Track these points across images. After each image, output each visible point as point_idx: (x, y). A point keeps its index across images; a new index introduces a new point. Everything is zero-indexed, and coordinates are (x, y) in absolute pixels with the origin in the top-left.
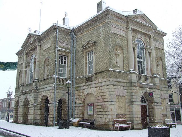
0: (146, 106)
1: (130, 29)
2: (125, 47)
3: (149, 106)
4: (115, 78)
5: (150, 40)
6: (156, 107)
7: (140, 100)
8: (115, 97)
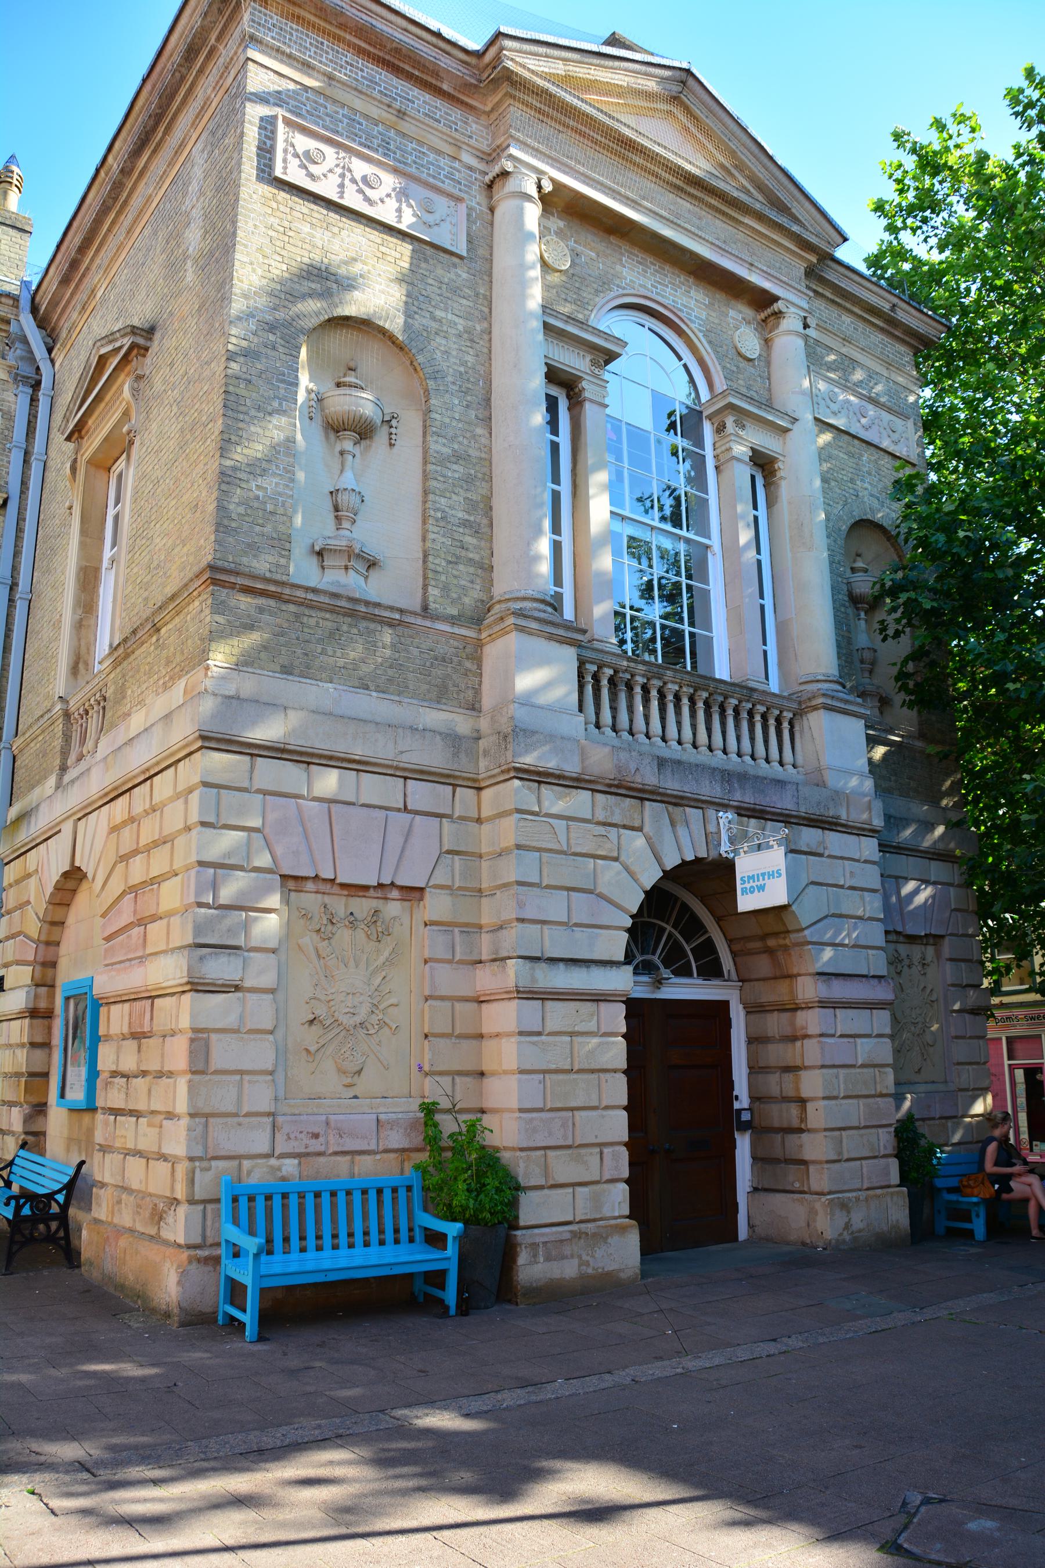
2: (447, 353)
3: (753, 1009)
4: (287, 670)
5: (767, 342)
6: (800, 997)
7: (616, 945)
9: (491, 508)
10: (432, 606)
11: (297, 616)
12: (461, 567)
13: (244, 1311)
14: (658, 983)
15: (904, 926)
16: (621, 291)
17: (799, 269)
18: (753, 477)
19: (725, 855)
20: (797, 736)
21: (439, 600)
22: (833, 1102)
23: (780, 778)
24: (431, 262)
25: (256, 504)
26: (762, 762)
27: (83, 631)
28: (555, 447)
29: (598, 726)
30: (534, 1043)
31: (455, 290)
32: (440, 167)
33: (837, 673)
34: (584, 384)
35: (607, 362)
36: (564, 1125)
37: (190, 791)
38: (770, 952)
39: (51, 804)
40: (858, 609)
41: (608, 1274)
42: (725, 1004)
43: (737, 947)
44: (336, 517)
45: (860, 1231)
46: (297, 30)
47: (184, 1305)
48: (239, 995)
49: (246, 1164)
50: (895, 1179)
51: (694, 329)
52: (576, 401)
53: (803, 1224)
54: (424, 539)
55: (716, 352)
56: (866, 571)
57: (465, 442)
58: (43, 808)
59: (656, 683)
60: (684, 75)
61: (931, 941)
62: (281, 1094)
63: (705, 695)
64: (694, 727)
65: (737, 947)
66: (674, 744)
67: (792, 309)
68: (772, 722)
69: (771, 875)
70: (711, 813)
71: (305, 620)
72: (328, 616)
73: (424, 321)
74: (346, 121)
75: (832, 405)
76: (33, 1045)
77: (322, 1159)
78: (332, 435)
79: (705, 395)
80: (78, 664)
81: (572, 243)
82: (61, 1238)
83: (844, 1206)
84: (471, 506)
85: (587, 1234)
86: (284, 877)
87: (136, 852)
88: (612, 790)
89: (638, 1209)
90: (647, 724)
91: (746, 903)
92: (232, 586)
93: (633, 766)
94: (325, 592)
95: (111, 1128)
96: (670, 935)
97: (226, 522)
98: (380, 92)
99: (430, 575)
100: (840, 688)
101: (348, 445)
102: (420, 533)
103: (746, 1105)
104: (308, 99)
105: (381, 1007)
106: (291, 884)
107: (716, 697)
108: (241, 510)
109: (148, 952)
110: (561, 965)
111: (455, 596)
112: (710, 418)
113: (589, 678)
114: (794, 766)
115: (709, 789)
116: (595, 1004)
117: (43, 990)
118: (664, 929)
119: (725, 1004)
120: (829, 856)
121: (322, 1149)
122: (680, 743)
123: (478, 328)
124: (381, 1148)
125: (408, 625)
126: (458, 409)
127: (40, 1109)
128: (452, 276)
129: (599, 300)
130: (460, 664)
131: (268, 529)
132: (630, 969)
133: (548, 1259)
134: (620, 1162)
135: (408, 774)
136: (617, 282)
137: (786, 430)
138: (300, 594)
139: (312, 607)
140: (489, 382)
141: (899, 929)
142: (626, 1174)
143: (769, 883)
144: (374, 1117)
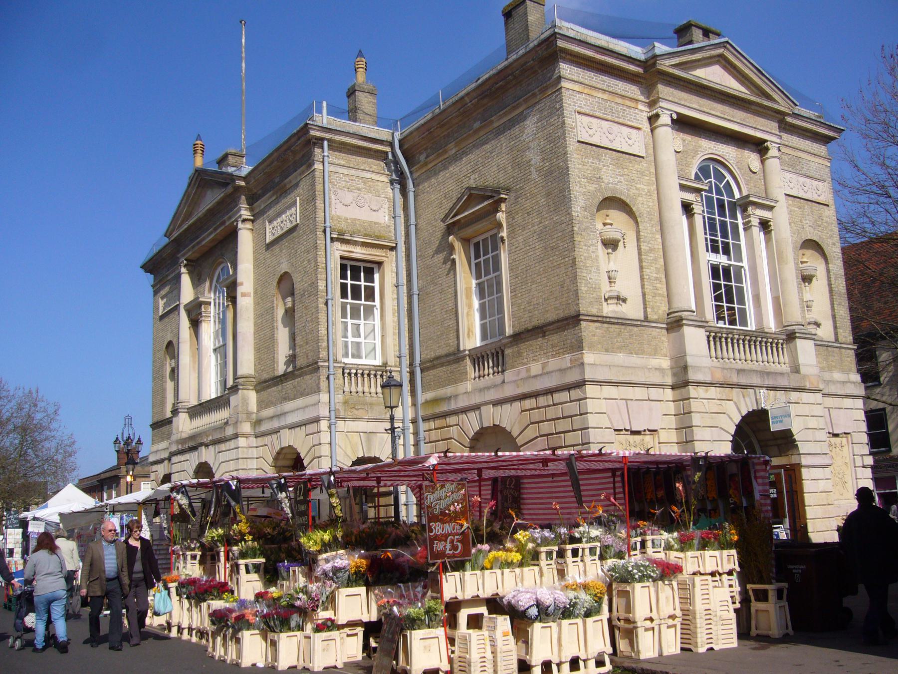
1: (665, 119)
2: (643, 205)
4: (607, 351)
5: (763, 162)
31: (642, 173)
34: (694, 206)
59: (730, 336)
70: (757, 389)
86: (615, 430)
101: (610, 251)
115: (756, 380)
119: (469, 616)
137: (773, 207)
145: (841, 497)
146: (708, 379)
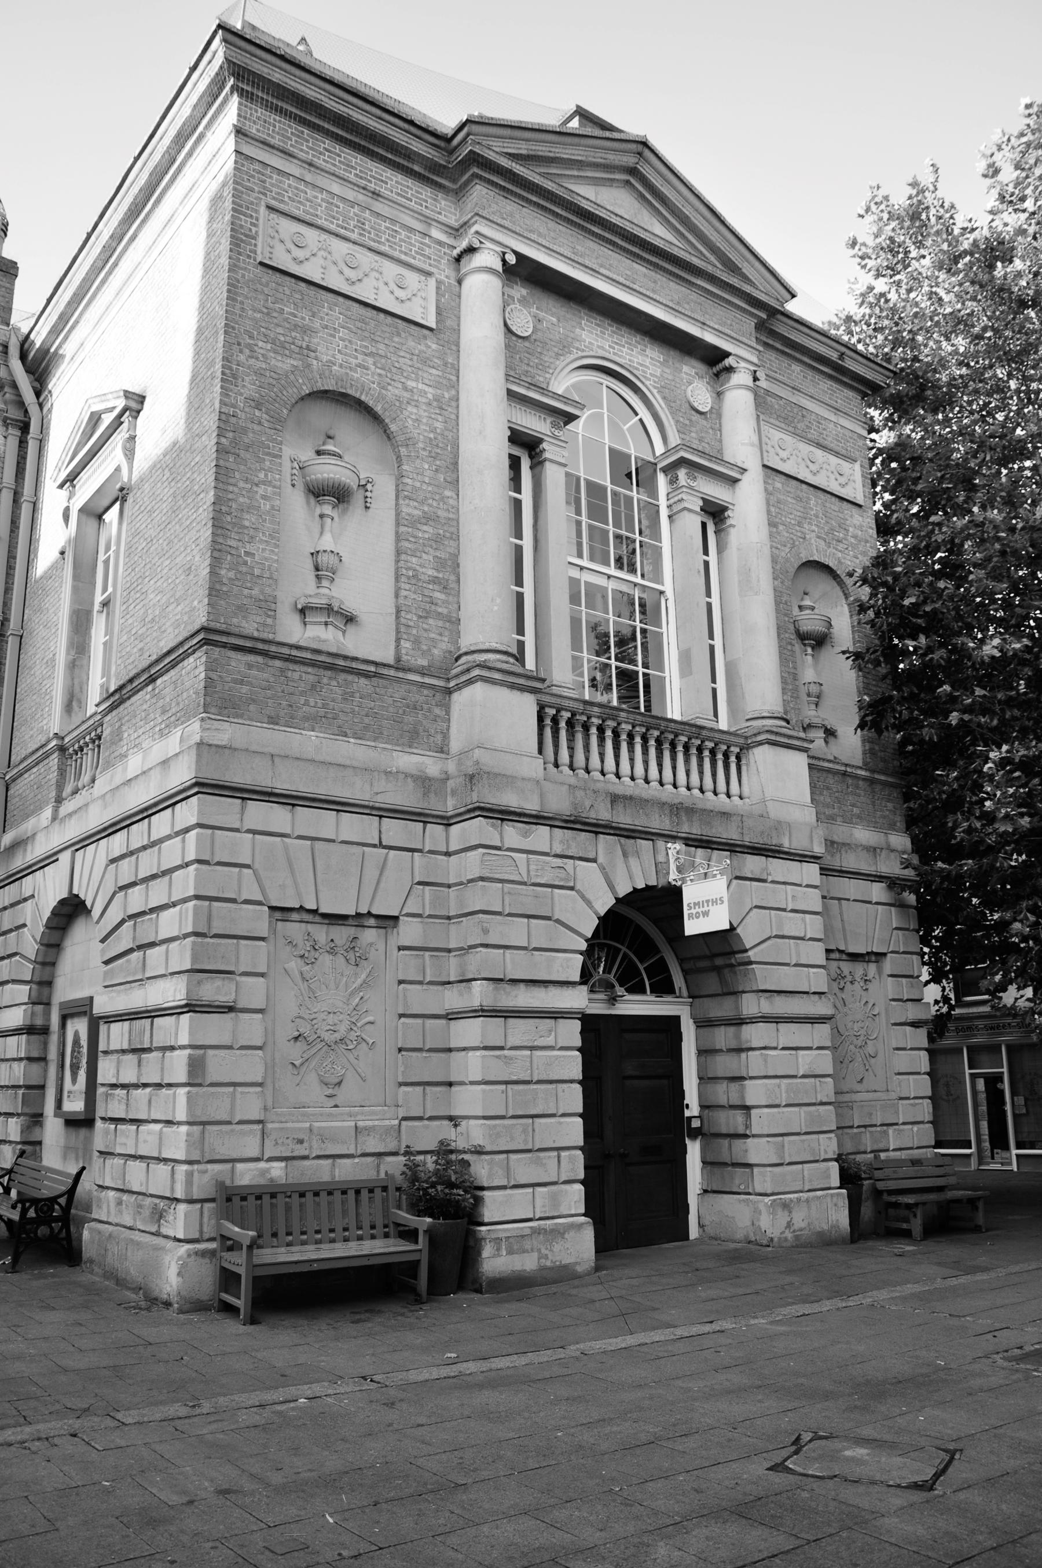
0: (674, 1022)
1: (487, 258)
2: (414, 421)
3: (703, 1024)
4: (273, 720)
7: (572, 966)
8: (259, 921)
9: (458, 565)
10: (405, 658)
11: (282, 670)
12: (431, 621)
13: (239, 1299)
14: (613, 1000)
15: (846, 944)
16: (580, 354)
17: (751, 323)
18: (704, 526)
19: (674, 883)
20: (744, 768)
21: (411, 652)
22: (775, 1110)
23: (726, 809)
24: (403, 335)
25: (244, 569)
26: (710, 795)
27: (77, 671)
28: (517, 504)
29: (556, 765)
30: (497, 1057)
31: (425, 361)
32: (411, 244)
33: (781, 710)
35: (566, 424)
36: (525, 1131)
37: (187, 830)
38: (718, 969)
39: (44, 830)
40: (805, 645)
41: (565, 1267)
42: (676, 1019)
43: (686, 966)
44: (317, 576)
45: (801, 1230)
46: (280, 122)
47: (184, 1293)
48: (233, 1015)
49: (239, 1166)
50: (836, 1181)
51: (649, 387)
52: (538, 462)
53: (749, 1223)
54: (397, 596)
55: (670, 407)
56: (813, 608)
57: (435, 504)
58: (40, 837)
59: (611, 723)
60: (640, 147)
61: (873, 958)
62: (270, 1104)
63: (656, 733)
64: (646, 763)
65: (686, 966)
66: (627, 780)
67: (743, 364)
68: (720, 756)
69: (714, 902)
70: (660, 843)
71: (289, 674)
72: (310, 670)
73: (397, 392)
74: (324, 204)
75: (781, 452)
76: (30, 1059)
77: (306, 1163)
78: (312, 500)
79: (660, 449)
80: (73, 701)
81: (534, 310)
82: (63, 1239)
83: (786, 1206)
84: (440, 564)
85: (545, 1230)
86: (273, 909)
87: (133, 884)
88: (569, 825)
89: (594, 1208)
90: (602, 761)
91: (691, 927)
92: (224, 645)
93: (587, 804)
94: (306, 649)
95: (111, 1136)
96: (625, 955)
97: (218, 587)
98: (356, 175)
99: (403, 629)
100: (784, 724)
102: (393, 591)
103: (696, 1114)
104: (289, 186)
105: (359, 1025)
106: (278, 915)
107: (667, 735)
108: (231, 574)
109: (148, 975)
110: (522, 986)
111: (425, 648)
112: (665, 470)
113: (548, 721)
114: (741, 798)
115: (658, 822)
116: (553, 1021)
117: (39, 1008)
118: (620, 950)
119: (676, 1019)
120: (773, 882)
121: (306, 1153)
122: (633, 778)
123: (447, 395)
124: (359, 1152)
125: (381, 676)
126: (428, 473)
127: (36, 1119)
128: (422, 348)
129: (560, 364)
130: (429, 710)
131: (255, 592)
132: (584, 988)
133: (510, 1252)
134: (575, 1164)
135: (383, 813)
136: (577, 344)
137: (736, 481)
138: (286, 651)
139: (296, 662)
140: (456, 446)
141: (842, 948)
142: (581, 1175)
143: (713, 909)
144: (353, 1124)
145: (859, 1087)
146: (532, 805)
